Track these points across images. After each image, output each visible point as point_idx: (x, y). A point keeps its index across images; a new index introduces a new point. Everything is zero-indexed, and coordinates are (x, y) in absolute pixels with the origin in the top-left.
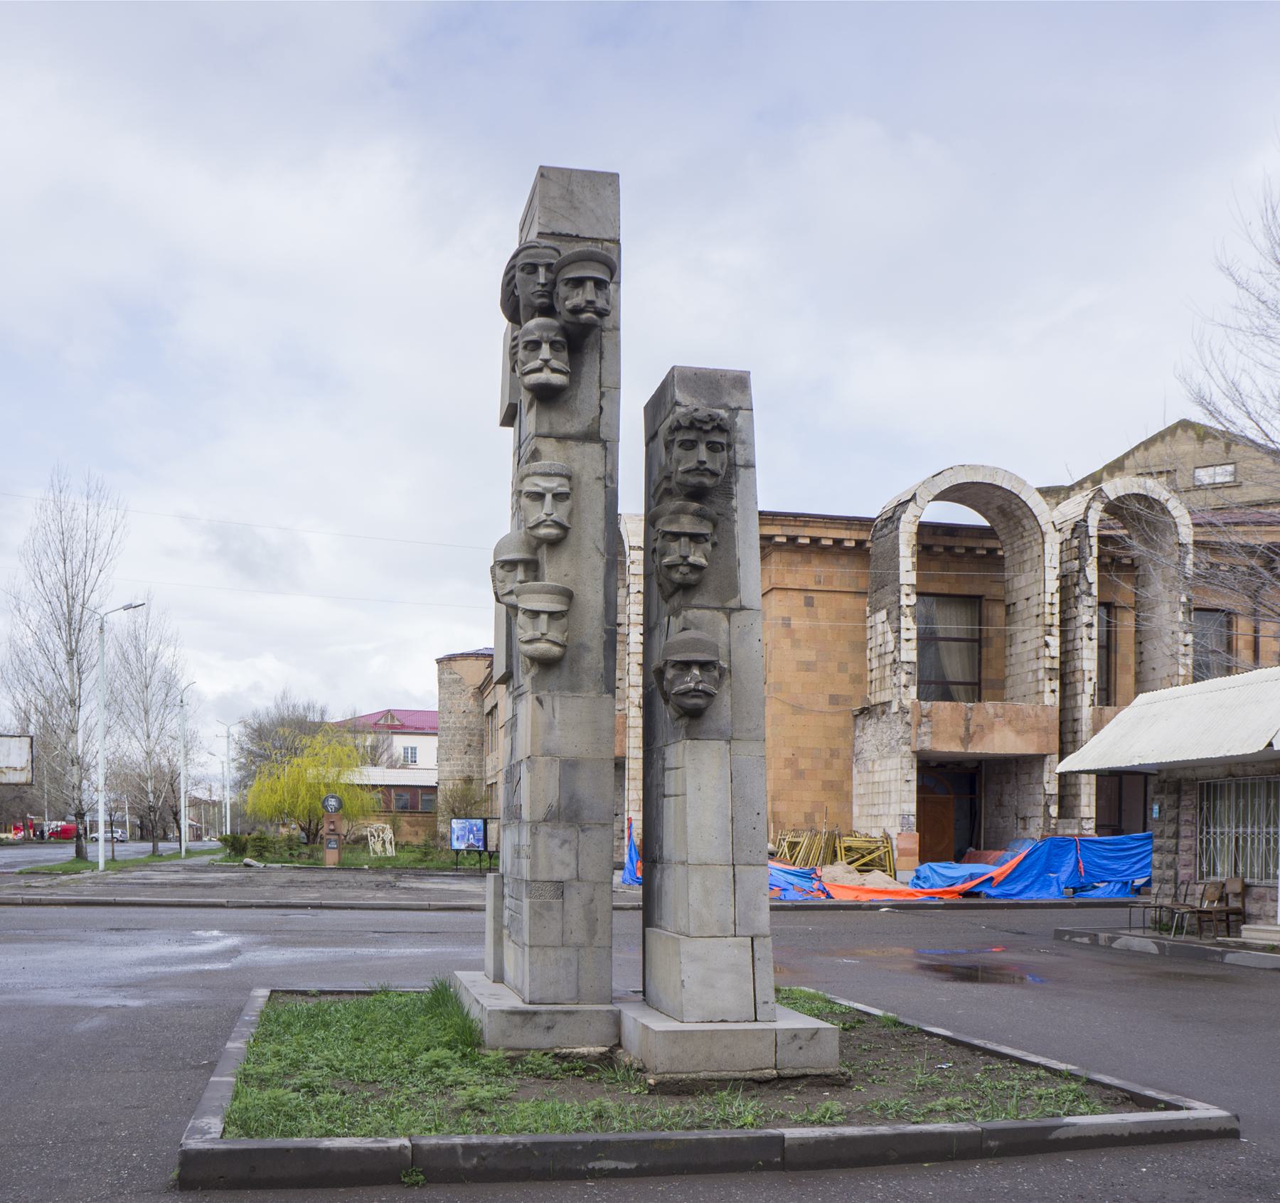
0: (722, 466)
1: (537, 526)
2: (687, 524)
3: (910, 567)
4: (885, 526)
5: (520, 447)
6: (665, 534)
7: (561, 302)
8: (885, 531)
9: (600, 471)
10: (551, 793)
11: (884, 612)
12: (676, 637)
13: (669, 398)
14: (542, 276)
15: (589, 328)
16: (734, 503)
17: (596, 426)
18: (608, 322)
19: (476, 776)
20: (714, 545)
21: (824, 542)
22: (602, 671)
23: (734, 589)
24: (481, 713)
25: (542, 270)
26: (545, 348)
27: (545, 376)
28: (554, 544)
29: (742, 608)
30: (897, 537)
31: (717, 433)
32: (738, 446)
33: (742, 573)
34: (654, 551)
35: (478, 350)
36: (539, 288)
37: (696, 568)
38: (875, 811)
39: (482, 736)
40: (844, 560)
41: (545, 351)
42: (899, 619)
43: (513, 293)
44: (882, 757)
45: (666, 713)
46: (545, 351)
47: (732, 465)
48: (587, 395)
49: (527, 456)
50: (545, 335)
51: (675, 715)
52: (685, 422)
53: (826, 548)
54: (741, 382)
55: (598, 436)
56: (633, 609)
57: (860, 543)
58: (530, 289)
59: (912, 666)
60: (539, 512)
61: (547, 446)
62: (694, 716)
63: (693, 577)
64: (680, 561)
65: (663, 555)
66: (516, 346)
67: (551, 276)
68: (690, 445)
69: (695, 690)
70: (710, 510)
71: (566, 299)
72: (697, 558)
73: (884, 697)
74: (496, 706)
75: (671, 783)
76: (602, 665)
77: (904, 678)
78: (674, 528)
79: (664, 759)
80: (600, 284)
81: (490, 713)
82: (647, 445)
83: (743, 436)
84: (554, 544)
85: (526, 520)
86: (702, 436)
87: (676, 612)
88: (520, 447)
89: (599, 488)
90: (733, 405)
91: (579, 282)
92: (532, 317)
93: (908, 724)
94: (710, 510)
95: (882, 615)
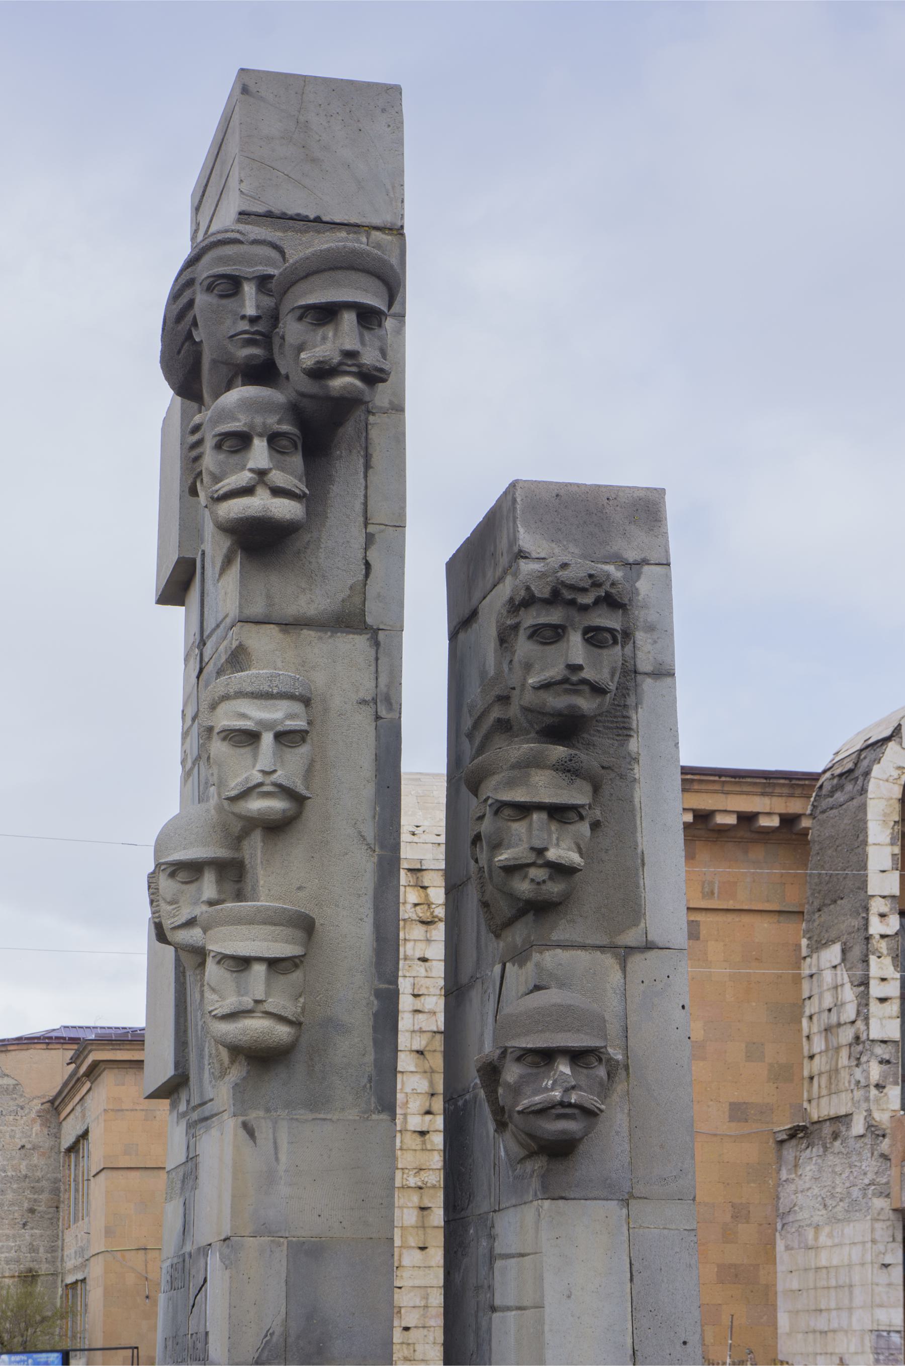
0: (613, 675)
1: (245, 794)
2: (544, 788)
3: (887, 864)
4: (840, 787)
5: (203, 643)
6: (501, 807)
7: (282, 353)
8: (839, 797)
9: (367, 688)
10: (270, 1308)
11: (836, 948)
12: (517, 1003)
13: (503, 544)
14: (250, 301)
15: (345, 407)
16: (633, 745)
17: (357, 600)
18: (381, 395)
19: (44, 1268)
20: (595, 826)
21: (720, 819)
22: (370, 1069)
23: (632, 908)
24: (55, 1148)
25: (249, 290)
26: (260, 446)
27: (261, 503)
28: (276, 828)
29: (649, 947)
30: (863, 808)
31: (603, 609)
32: (640, 636)
33: (648, 879)
34: (477, 839)
35: (110, 451)
36: (244, 326)
37: (561, 870)
38: (821, 1323)
39: (56, 1192)
40: (758, 852)
41: (260, 454)
42: (866, 961)
43: (189, 336)
44: (834, 1220)
45: (496, 1148)
46: (260, 454)
47: (630, 673)
48: (340, 537)
49: (214, 663)
50: (259, 420)
51: (518, 1151)
52: (542, 590)
53: (723, 830)
54: (647, 509)
55: (365, 621)
56: (424, 955)
57: (789, 821)
58: (224, 328)
59: (890, 1048)
60: (244, 769)
61: (263, 641)
62: (556, 1152)
63: (555, 888)
64: (531, 858)
65: (496, 846)
66: (199, 443)
67: (268, 302)
68: (550, 635)
69: (562, 1104)
70: (588, 759)
71: (301, 348)
72: (562, 852)
73: (837, 1106)
74: (85, 1135)
75: (508, 1283)
76: (370, 1058)
77: (875, 1071)
78: (519, 795)
79: (492, 1238)
80: (368, 318)
81: (73, 1149)
82: (453, 636)
83: (652, 616)
84: (276, 828)
85: (221, 784)
86: (566, 620)
87: (520, 956)
88: (203, 643)
89: (363, 720)
90: (632, 555)
91: (326, 314)
92: (229, 387)
93: (885, 1157)
94: (588, 759)
95: (833, 953)
